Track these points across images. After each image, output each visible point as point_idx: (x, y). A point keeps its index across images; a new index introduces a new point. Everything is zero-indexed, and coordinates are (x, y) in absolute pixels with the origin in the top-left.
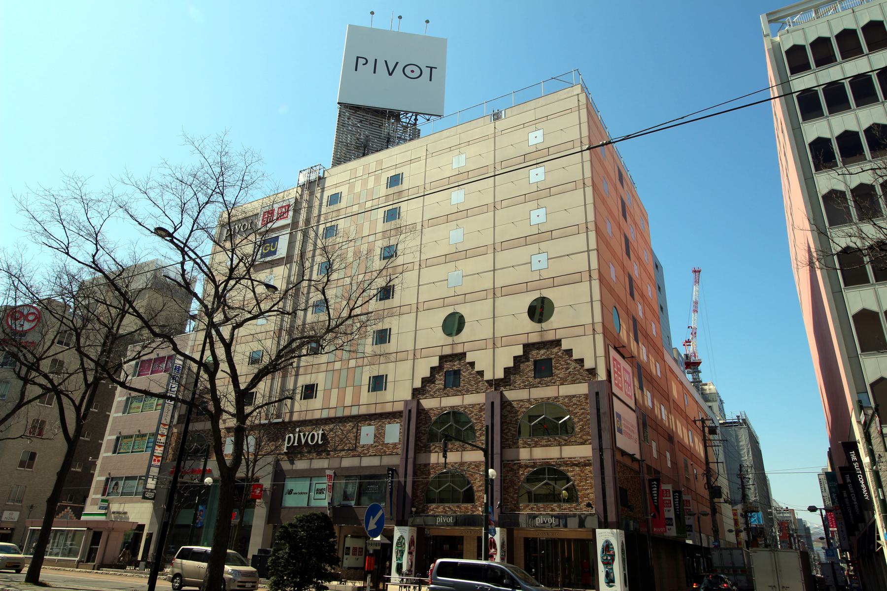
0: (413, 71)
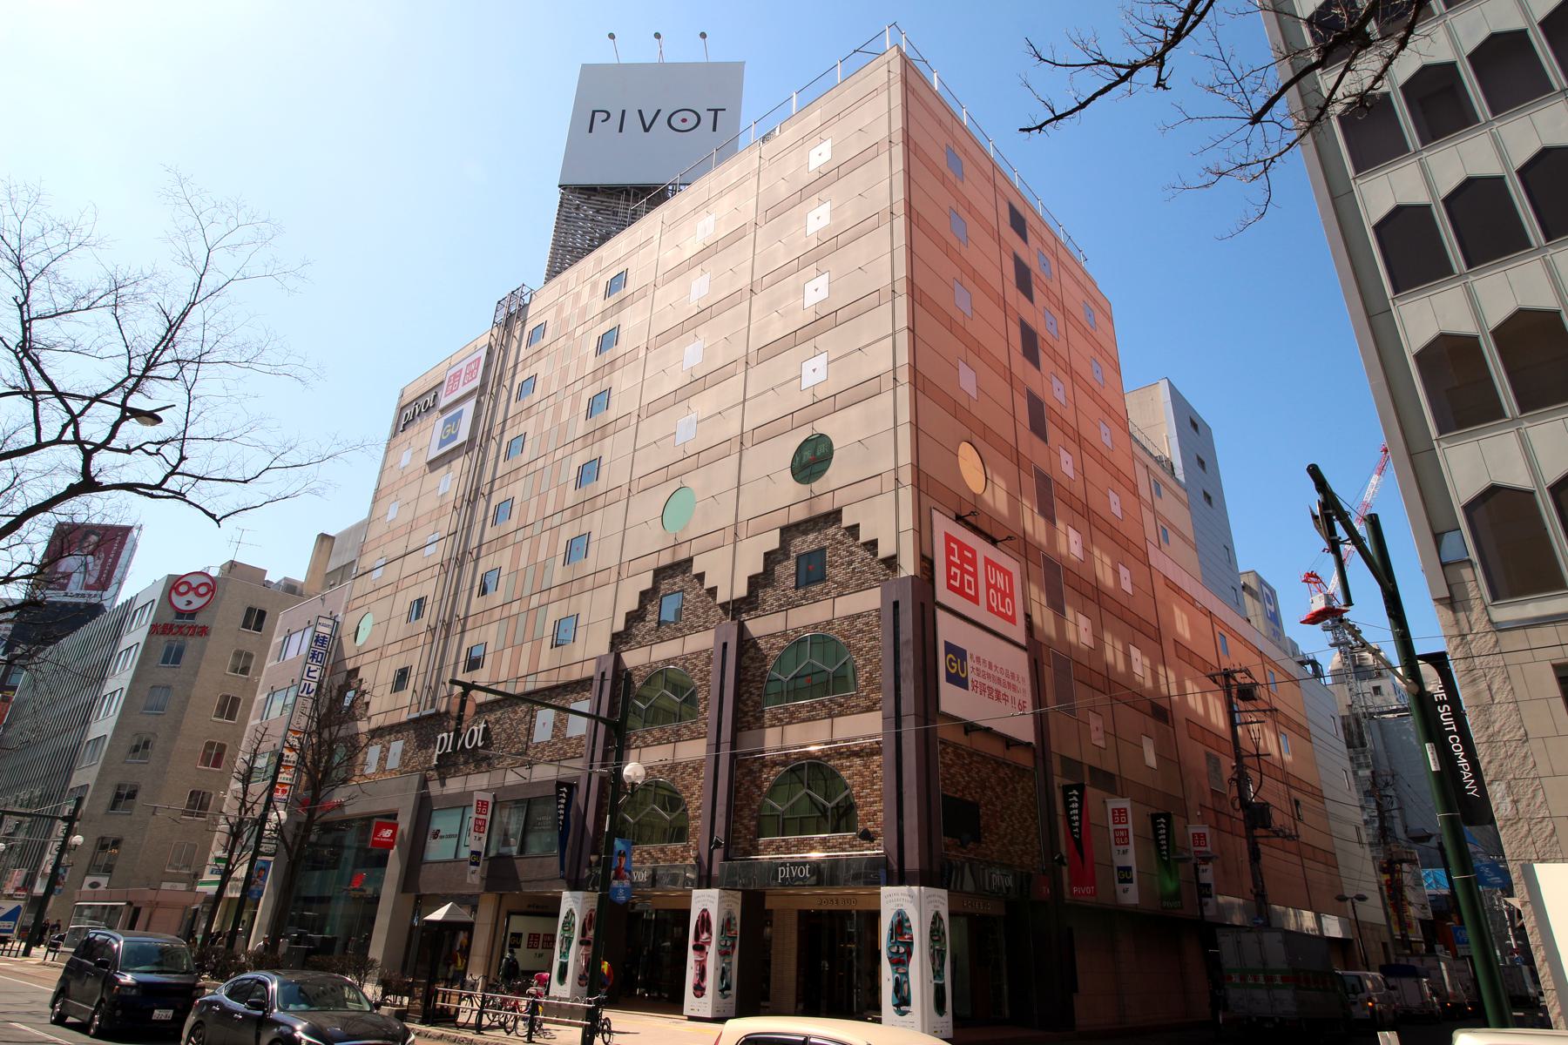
0: (684, 120)
